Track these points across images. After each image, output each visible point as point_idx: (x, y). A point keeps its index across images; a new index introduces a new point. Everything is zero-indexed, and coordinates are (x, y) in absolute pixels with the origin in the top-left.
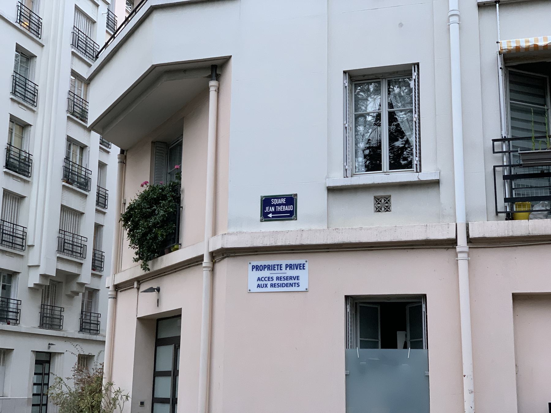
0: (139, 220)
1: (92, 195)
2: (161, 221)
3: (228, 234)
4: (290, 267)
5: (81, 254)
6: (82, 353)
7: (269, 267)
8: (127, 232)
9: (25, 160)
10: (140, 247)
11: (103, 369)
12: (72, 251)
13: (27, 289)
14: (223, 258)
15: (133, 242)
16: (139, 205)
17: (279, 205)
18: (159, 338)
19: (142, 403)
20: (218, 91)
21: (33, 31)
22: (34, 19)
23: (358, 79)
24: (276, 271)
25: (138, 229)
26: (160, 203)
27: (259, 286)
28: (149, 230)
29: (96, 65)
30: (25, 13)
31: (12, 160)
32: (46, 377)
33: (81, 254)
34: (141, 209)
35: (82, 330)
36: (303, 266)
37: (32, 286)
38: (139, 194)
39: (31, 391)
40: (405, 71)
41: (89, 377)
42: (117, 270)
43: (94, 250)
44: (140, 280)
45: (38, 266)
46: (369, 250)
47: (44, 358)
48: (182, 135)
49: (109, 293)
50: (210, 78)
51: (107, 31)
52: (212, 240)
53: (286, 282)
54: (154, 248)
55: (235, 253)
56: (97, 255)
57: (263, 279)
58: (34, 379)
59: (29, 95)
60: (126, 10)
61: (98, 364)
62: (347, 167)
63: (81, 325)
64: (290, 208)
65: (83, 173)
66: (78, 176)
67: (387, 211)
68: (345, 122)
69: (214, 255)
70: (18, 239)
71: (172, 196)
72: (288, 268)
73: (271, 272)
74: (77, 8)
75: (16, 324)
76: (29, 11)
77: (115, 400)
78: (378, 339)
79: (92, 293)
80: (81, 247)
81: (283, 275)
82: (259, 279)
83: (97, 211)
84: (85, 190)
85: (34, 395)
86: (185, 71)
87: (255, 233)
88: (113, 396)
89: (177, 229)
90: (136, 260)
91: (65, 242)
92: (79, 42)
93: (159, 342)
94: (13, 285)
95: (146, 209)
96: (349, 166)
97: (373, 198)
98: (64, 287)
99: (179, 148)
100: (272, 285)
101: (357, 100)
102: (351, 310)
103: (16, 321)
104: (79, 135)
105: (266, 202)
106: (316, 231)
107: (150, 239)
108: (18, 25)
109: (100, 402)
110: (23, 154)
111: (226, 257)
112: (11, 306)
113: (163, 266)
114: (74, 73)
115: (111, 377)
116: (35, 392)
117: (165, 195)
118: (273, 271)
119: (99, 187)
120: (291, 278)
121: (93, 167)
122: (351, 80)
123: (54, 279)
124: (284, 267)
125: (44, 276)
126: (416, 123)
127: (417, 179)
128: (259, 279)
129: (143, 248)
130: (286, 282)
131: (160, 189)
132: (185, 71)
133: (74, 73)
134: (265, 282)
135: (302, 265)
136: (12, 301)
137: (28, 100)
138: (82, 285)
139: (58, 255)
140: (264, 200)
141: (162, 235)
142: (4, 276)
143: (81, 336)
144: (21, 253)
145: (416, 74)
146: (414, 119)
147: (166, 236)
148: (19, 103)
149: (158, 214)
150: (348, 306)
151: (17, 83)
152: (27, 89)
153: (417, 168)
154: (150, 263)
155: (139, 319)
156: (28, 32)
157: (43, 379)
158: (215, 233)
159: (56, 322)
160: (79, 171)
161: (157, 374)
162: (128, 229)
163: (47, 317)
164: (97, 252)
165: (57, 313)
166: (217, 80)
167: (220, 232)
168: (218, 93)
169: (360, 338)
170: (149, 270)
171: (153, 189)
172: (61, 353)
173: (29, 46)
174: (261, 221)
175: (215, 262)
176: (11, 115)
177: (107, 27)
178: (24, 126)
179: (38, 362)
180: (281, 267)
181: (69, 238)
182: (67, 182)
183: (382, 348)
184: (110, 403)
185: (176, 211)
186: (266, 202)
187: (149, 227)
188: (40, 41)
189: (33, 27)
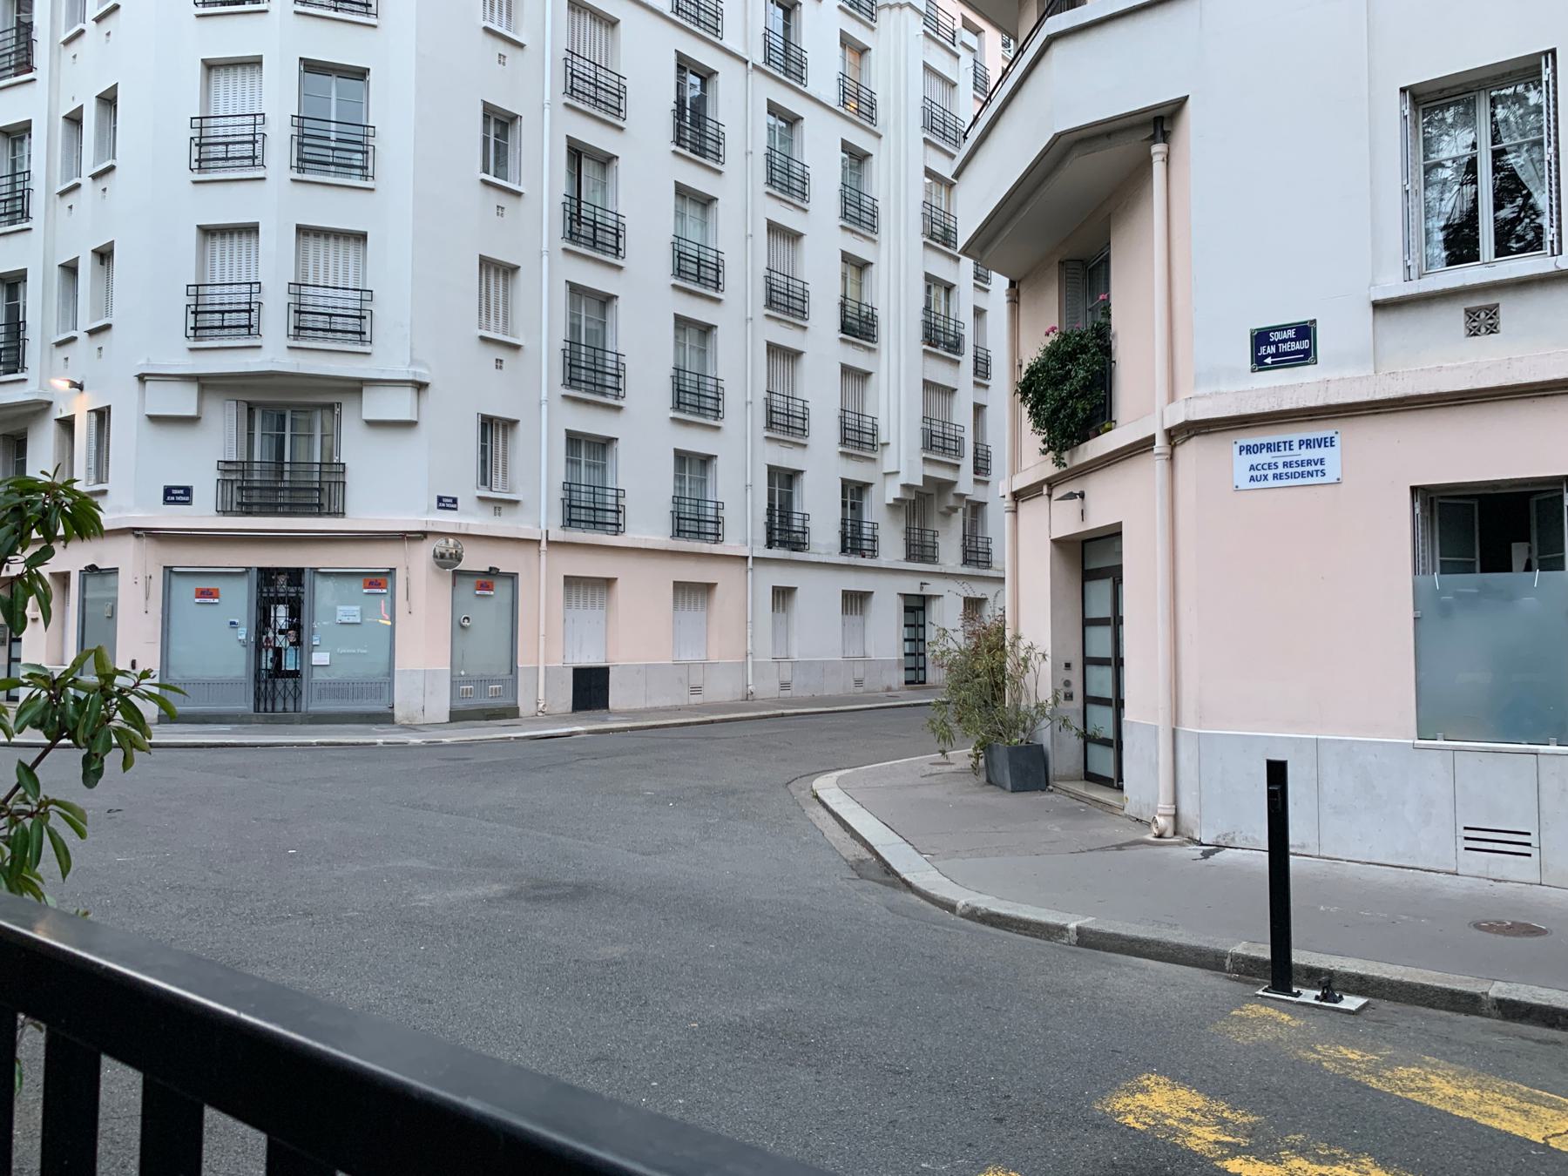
0: (1046, 389)
1: (967, 360)
2: (1082, 388)
3: (1197, 397)
4: (1308, 444)
5: (956, 451)
6: (972, 596)
7: (1269, 447)
8: (1027, 409)
9: (867, 317)
10: (1048, 431)
11: (1004, 616)
12: (944, 448)
13: (884, 507)
14: (1189, 438)
15: (1037, 424)
16: (1044, 365)
17: (1284, 341)
18: (1086, 568)
19: (1068, 666)
20: (1167, 160)
21: (863, 116)
22: (864, 95)
23: (1428, 98)
24: (1283, 453)
25: (1044, 403)
26: (1079, 359)
27: (1252, 479)
28: (1063, 403)
29: (961, 155)
30: (851, 88)
31: (849, 320)
32: (921, 630)
33: (956, 451)
34: (1048, 371)
35: (966, 562)
36: (1332, 442)
37: (891, 502)
38: (1042, 348)
39: (901, 649)
40: (1525, 69)
41: (984, 628)
42: (1015, 470)
43: (976, 444)
44: (1051, 483)
45: (898, 473)
46: (1455, 405)
47: (915, 603)
48: (1109, 244)
49: (1006, 505)
50: (1153, 139)
51: (975, 97)
52: (1169, 409)
53: (1300, 469)
54: (1071, 431)
55: (1209, 427)
56: (980, 452)
57: (1259, 467)
58: (904, 632)
59: (866, 217)
60: (1004, 57)
61: (997, 610)
62: (1409, 263)
63: (965, 554)
64: (1305, 344)
65: (952, 328)
66: (944, 334)
67: (1492, 332)
68: (1405, 182)
69: (1173, 433)
70: (867, 436)
71: (1098, 345)
72: (1304, 447)
73: (1274, 454)
74: (926, 67)
75: (873, 557)
76: (855, 85)
77: (1025, 660)
78: (1474, 557)
79: (977, 508)
80: (956, 441)
81: (1295, 459)
82: (1252, 468)
83: (976, 384)
84: (955, 353)
85: (906, 655)
86: (1109, 134)
87: (1243, 392)
88: (1022, 654)
89: (1108, 397)
90: (1044, 452)
91: (932, 436)
92: (934, 121)
93: (1088, 576)
94: (865, 502)
95: (1055, 370)
96: (1414, 260)
97: (1463, 312)
98: (935, 501)
99: (1103, 267)
100: (1275, 476)
101: (1427, 142)
102: (1422, 511)
103: (874, 553)
104: (942, 268)
105: (1260, 338)
106: (1354, 380)
107: (1065, 417)
108: (842, 110)
109: (1004, 662)
110: (864, 309)
111: (1193, 436)
112: (865, 531)
113: (1088, 458)
114: (929, 173)
115: (1017, 627)
116: (907, 651)
117: (1086, 345)
118: (1277, 454)
119: (976, 347)
120: (1309, 462)
121: (966, 317)
122: (1416, 103)
123: (919, 490)
124: (1296, 445)
125: (906, 487)
126: (1550, 163)
127: (1553, 269)
128: (1252, 468)
129: (1054, 432)
130: (1300, 469)
131: (1077, 336)
132: (1109, 134)
133: (929, 173)
134: (1263, 472)
135: (1328, 440)
136: (865, 525)
137: (865, 225)
138: (961, 496)
139: (924, 455)
140: (1256, 336)
141: (1084, 410)
142: (852, 490)
143: (966, 570)
144: (873, 456)
145: (1549, 70)
146: (1547, 158)
147: (1091, 410)
148: (853, 231)
149: (1076, 376)
150: (1417, 505)
151: (575, 73)
152: (599, 84)
153: (1552, 248)
154: (1066, 455)
155: (1054, 541)
156: (857, 119)
157: (917, 633)
158: (1172, 398)
159: (929, 551)
160: (946, 325)
161: (1087, 623)
162: (1029, 405)
163: (915, 545)
164: (980, 447)
165: (929, 539)
166: (1164, 142)
167: (1182, 395)
168: (1167, 164)
169: (1441, 556)
170: (1065, 465)
171: (1065, 337)
172: (939, 596)
173: (861, 140)
174: (1253, 371)
175: (1175, 445)
176: (842, 251)
177: (975, 89)
178: (862, 266)
179: (907, 609)
180: (1290, 446)
181: (937, 428)
182: (929, 345)
183: (1483, 571)
184: (1019, 665)
185: (1104, 369)
186: (1260, 338)
187: (1062, 399)
188: (875, 129)
189: (864, 108)
